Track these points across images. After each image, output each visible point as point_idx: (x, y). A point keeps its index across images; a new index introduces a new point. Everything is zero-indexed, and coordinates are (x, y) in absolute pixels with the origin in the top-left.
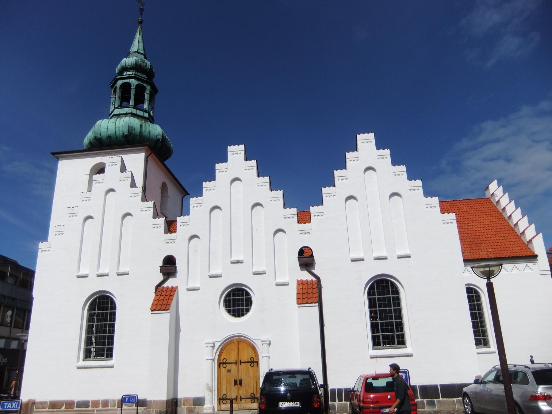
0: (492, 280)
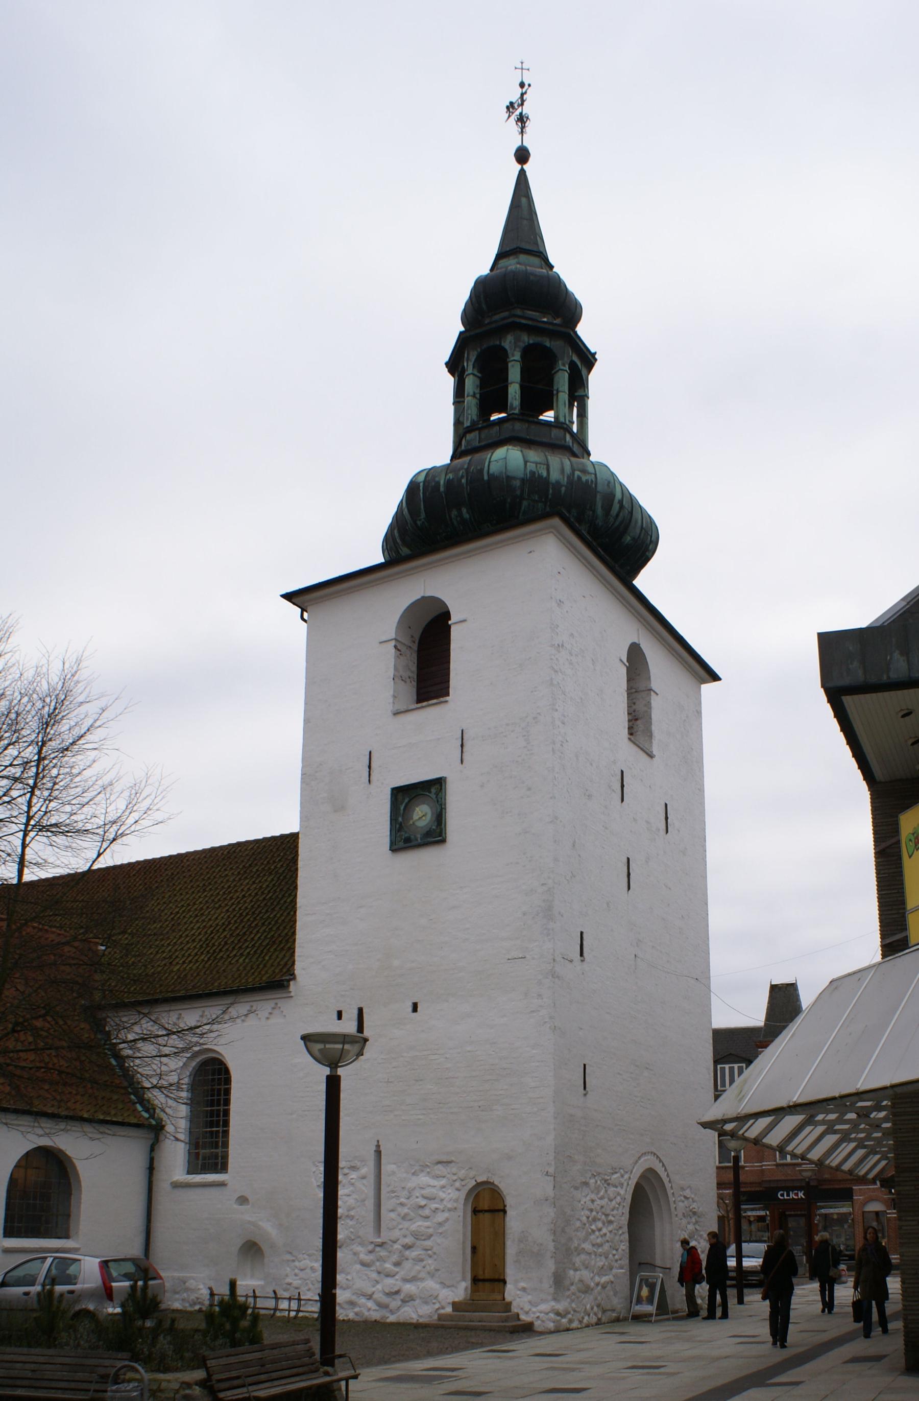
0: (340, 1071)
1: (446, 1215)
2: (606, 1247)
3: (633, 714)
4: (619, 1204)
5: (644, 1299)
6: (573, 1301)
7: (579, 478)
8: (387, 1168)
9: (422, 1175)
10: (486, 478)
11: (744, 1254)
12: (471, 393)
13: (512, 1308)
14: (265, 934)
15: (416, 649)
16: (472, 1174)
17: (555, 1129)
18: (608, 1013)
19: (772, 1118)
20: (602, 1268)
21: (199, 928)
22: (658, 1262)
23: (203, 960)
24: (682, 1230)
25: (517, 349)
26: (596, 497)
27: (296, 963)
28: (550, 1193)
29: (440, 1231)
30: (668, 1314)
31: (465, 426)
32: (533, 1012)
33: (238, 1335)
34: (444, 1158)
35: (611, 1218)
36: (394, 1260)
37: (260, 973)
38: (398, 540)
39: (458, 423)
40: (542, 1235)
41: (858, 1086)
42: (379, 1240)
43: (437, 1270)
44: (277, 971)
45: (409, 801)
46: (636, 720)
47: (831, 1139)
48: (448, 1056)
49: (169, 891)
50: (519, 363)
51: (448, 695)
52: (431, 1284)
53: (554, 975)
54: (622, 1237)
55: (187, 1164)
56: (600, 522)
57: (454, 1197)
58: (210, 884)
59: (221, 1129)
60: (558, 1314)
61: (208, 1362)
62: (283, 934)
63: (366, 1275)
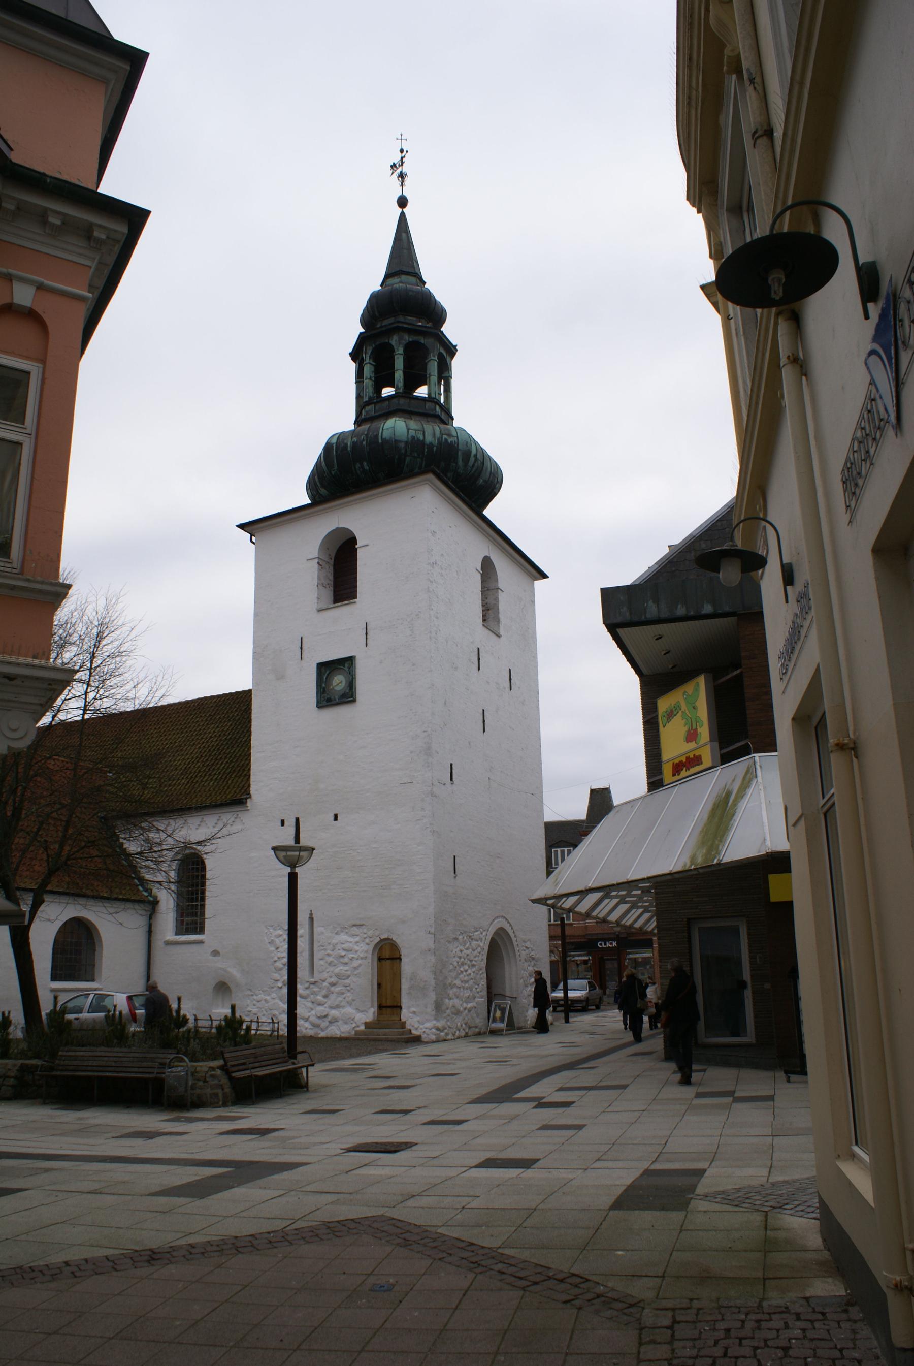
0: (297, 870)
1: (359, 962)
2: (471, 982)
3: (486, 606)
4: (480, 953)
5: (498, 1019)
6: (448, 1020)
7: (446, 440)
8: (317, 929)
9: (342, 934)
10: (380, 441)
11: (569, 988)
12: (369, 377)
13: (406, 1026)
14: (228, 765)
15: (333, 564)
16: (377, 933)
17: (434, 902)
18: (470, 819)
19: (578, 897)
20: (468, 997)
21: (179, 760)
22: (508, 994)
23: (184, 784)
24: (525, 970)
25: (401, 346)
26: (458, 452)
27: (251, 786)
28: (432, 946)
29: (356, 973)
30: (515, 1030)
31: (364, 400)
32: (418, 820)
33: (238, 1039)
34: (358, 922)
35: (474, 962)
36: (323, 994)
37: (225, 793)
38: (318, 483)
39: (359, 397)
40: (426, 975)
41: (628, 878)
42: (313, 980)
43: (354, 1000)
44: (237, 791)
45: (330, 673)
46: (488, 610)
47: (623, 908)
48: (359, 851)
49: (156, 733)
50: (402, 356)
51: (356, 598)
52: (349, 1010)
53: (433, 795)
54: (482, 976)
55: (175, 928)
56: (461, 471)
57: (366, 949)
58: (186, 727)
59: (199, 903)
60: (438, 1029)
61: (225, 1054)
62: (241, 765)
63: (304, 1004)
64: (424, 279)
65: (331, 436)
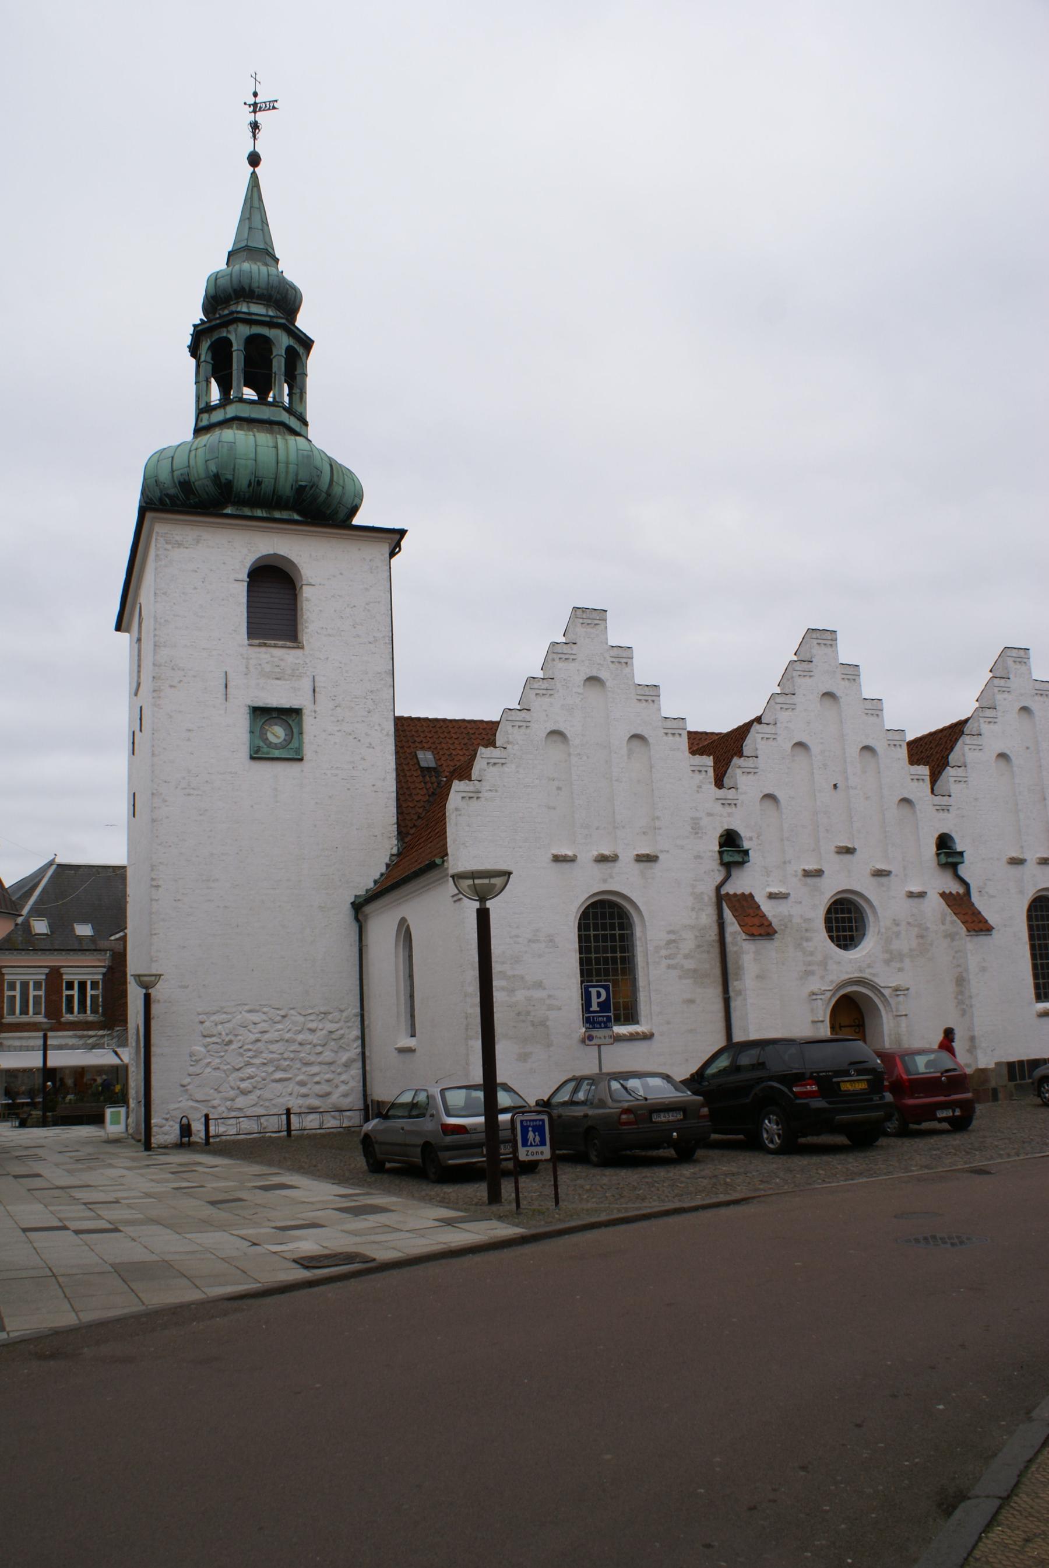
0: (489, 904)
64: (277, 256)
65: (148, 458)
